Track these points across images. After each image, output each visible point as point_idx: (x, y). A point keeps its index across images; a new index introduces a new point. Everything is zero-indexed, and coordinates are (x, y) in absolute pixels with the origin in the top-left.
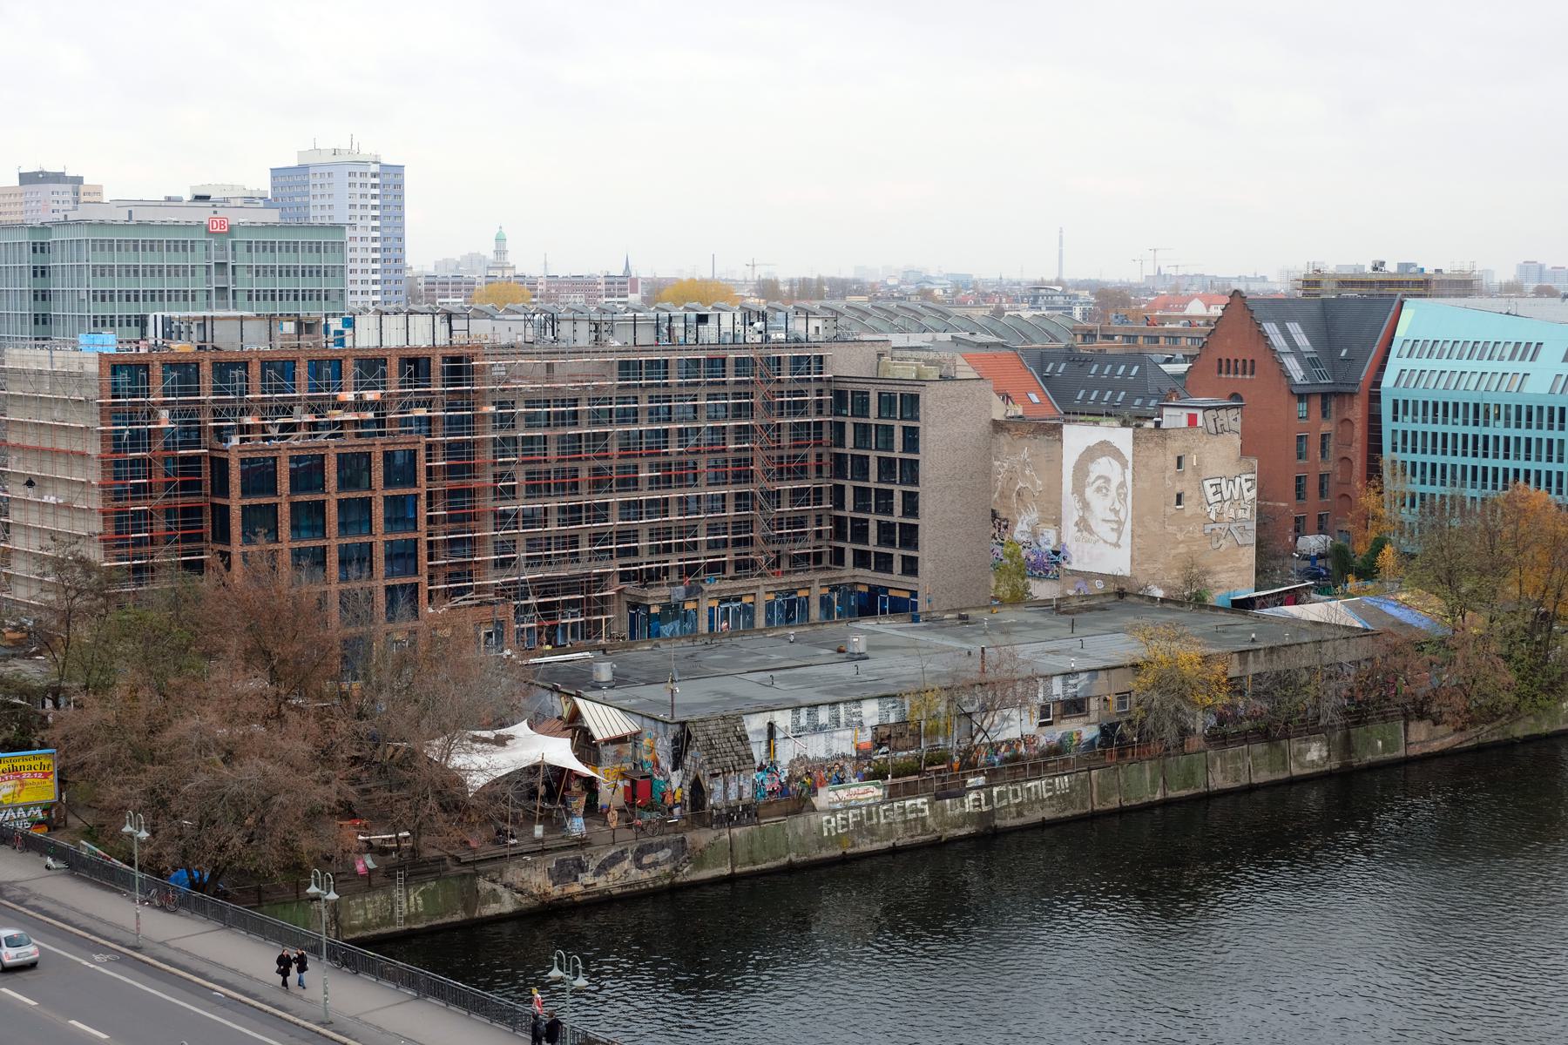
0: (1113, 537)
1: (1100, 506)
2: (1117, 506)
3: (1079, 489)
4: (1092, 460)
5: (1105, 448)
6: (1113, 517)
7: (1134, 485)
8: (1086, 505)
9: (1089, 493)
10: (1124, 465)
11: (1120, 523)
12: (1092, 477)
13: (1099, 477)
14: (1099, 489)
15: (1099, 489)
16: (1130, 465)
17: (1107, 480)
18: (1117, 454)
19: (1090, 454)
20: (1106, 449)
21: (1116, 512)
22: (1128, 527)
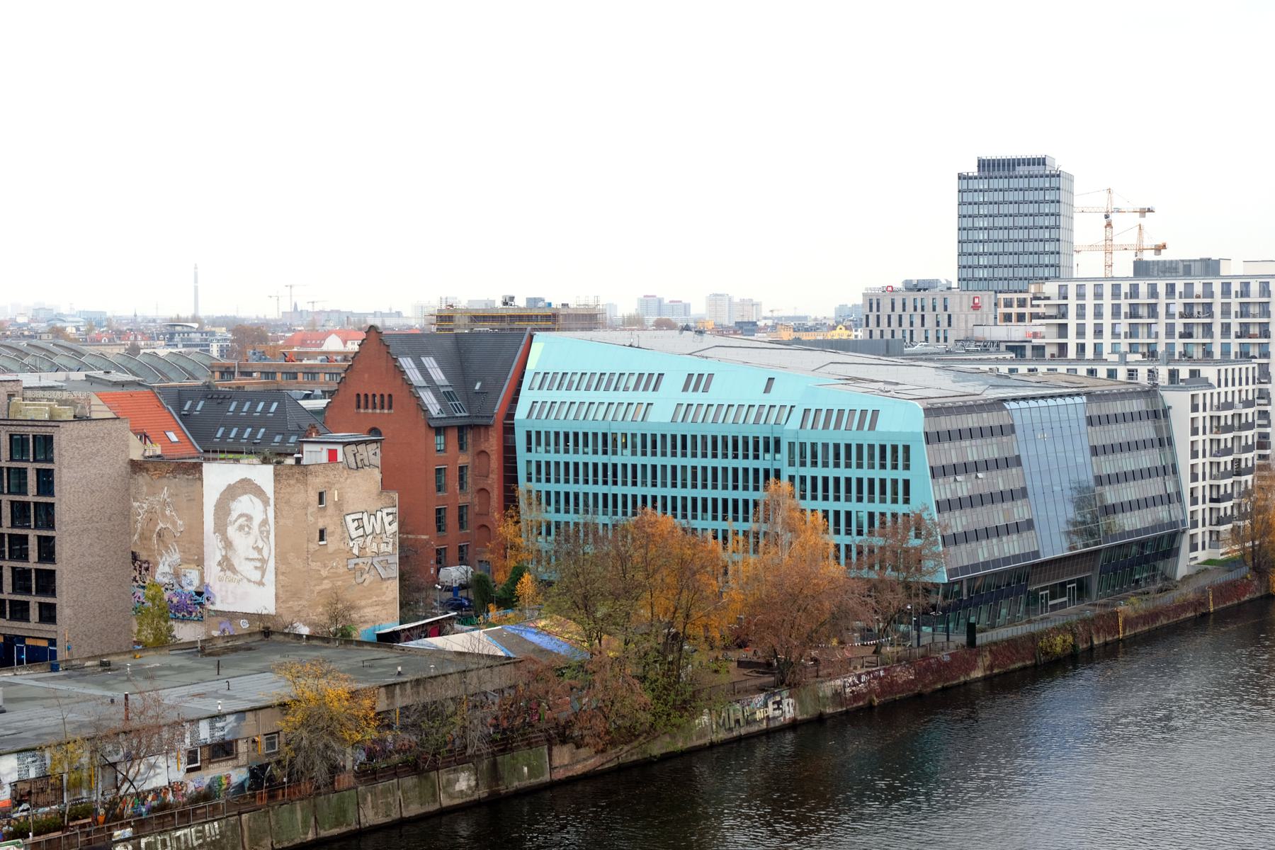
0: (256, 576)
1: (243, 544)
2: (260, 544)
3: (221, 528)
4: (234, 498)
5: (247, 486)
6: (256, 555)
7: (276, 522)
8: (228, 544)
9: (232, 532)
10: (266, 503)
11: (264, 561)
12: (234, 515)
13: (241, 516)
14: (241, 528)
15: (241, 528)
16: (272, 502)
17: (249, 518)
18: (258, 491)
19: (231, 493)
20: (247, 486)
21: (260, 550)
22: (271, 565)
